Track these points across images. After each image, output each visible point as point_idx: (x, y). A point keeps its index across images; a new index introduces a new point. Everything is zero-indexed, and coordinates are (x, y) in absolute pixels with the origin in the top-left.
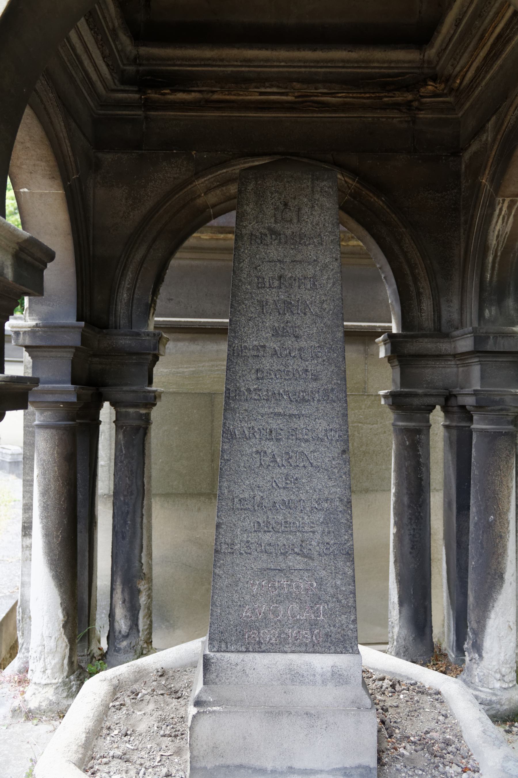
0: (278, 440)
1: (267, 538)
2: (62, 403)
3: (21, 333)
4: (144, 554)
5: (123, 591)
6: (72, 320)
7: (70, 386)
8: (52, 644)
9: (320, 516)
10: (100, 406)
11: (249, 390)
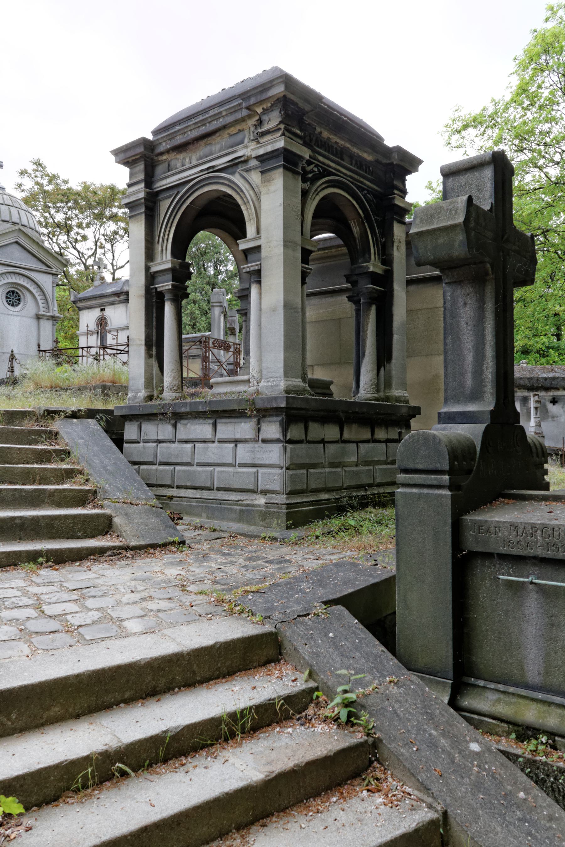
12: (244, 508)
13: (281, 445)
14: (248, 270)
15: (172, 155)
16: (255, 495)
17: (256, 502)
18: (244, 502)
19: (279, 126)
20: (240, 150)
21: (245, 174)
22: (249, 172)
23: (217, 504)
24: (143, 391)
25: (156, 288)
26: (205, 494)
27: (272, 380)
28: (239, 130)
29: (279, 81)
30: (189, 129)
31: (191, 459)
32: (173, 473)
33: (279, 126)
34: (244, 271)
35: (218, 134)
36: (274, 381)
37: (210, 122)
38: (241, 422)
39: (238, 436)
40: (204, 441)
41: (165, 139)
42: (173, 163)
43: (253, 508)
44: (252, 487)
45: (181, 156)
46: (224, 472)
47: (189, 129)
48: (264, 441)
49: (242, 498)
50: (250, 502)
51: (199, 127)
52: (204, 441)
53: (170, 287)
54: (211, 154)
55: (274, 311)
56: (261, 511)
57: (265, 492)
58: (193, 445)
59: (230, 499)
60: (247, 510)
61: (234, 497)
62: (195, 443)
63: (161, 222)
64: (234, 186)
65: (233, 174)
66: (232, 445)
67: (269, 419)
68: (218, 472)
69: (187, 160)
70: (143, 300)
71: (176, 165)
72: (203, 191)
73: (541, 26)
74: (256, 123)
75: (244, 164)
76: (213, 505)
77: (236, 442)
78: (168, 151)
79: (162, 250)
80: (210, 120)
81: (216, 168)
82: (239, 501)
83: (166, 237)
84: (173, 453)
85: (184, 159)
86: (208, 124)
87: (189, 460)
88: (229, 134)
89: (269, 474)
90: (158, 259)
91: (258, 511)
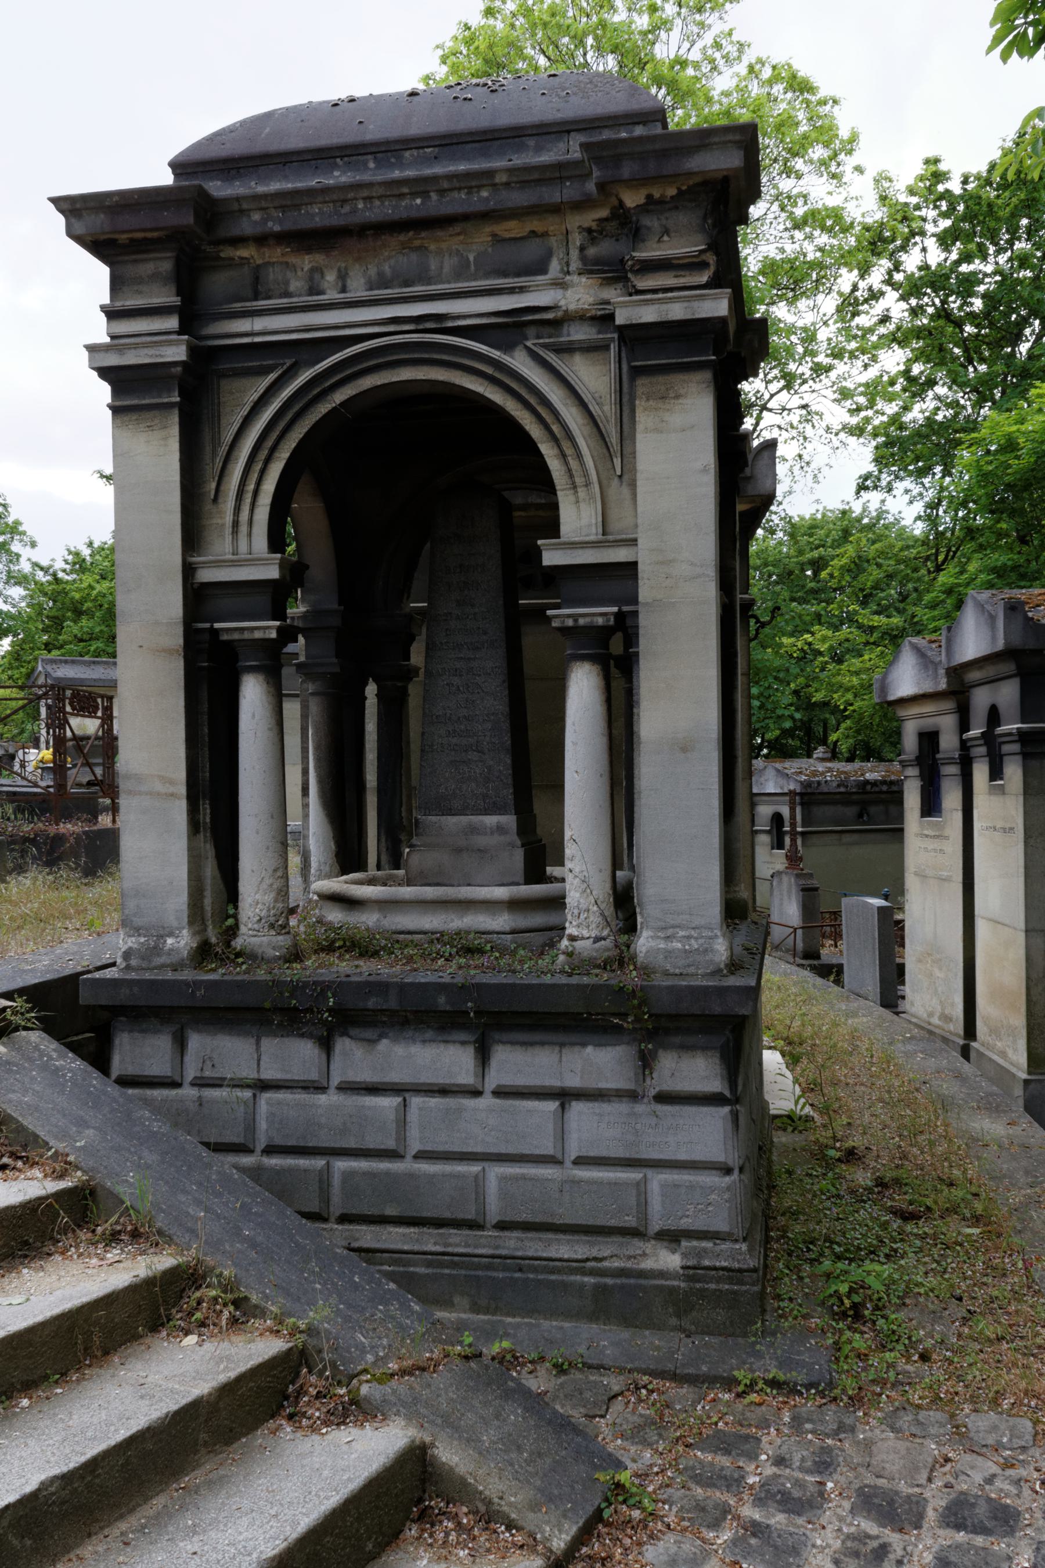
0: (461, 676)
1: (454, 741)
2: (329, 673)
3: (333, 1219)
4: (403, 809)
5: (386, 841)
6: (335, 606)
7: (335, 660)
8: (327, 869)
9: (489, 725)
10: (366, 684)
11: (441, 643)
12: (609, 1281)
13: (727, 1109)
14: (570, 623)
15: (275, 254)
16: (637, 1246)
17: (648, 1264)
18: (606, 1264)
19: (704, 257)
20: (538, 288)
21: (552, 358)
22: (566, 356)
23: (506, 1269)
24: (185, 932)
25: (216, 632)
26: (457, 1241)
27: (681, 933)
28: (533, 232)
29: (730, 137)
30: (365, 193)
31: (397, 1140)
32: (324, 1179)
33: (704, 257)
34: (555, 624)
35: (458, 228)
36: (689, 937)
37: (442, 192)
38: (584, 1045)
39: (573, 1082)
40: (444, 1091)
41: (264, 204)
42: (273, 275)
43: (643, 1282)
44: (630, 1221)
45: (306, 262)
46: (524, 1177)
47: (365, 193)
48: (664, 1098)
49: (594, 1252)
50: (629, 1265)
51: (401, 196)
52: (444, 1091)
53: (273, 635)
54: (425, 278)
55: (684, 750)
56: (672, 1290)
57: (671, 1237)
58: (400, 1099)
59: (553, 1254)
60: (622, 1287)
61: (565, 1249)
62: (407, 1095)
63: (228, 436)
64: (514, 385)
65: (508, 347)
66: (552, 1105)
67: (677, 1040)
68: (503, 1179)
69: (331, 277)
70: (177, 668)
71: (287, 283)
72: (395, 379)
73: (476, 20)
74: (594, 226)
75: (548, 330)
76: (495, 1274)
77: (564, 1096)
78: (262, 240)
79: (236, 524)
80: (446, 185)
81: (450, 324)
82: (587, 1260)
83: (251, 487)
84: (323, 1120)
85: (317, 271)
86: (434, 196)
87: (391, 1144)
88: (494, 235)
89: (691, 1187)
90: (220, 545)
91: (660, 1288)
